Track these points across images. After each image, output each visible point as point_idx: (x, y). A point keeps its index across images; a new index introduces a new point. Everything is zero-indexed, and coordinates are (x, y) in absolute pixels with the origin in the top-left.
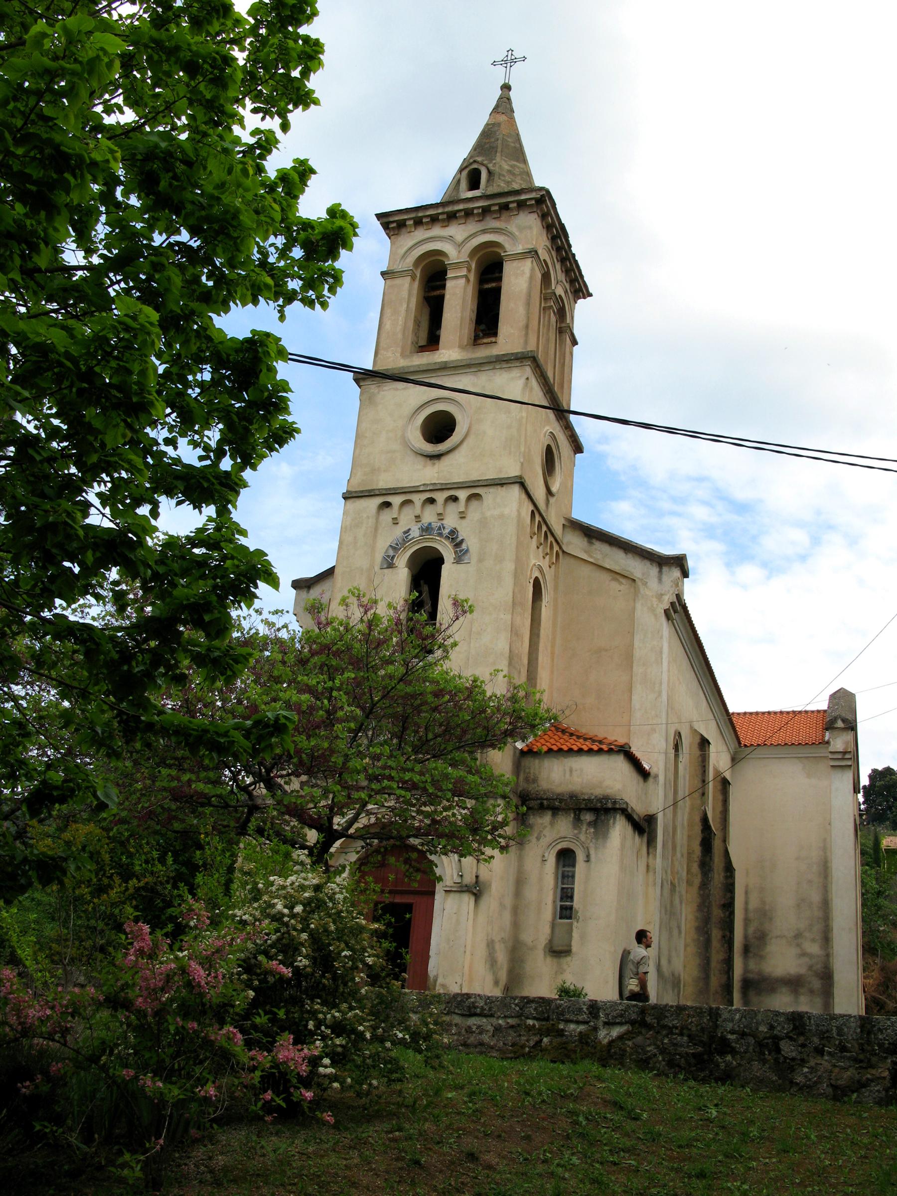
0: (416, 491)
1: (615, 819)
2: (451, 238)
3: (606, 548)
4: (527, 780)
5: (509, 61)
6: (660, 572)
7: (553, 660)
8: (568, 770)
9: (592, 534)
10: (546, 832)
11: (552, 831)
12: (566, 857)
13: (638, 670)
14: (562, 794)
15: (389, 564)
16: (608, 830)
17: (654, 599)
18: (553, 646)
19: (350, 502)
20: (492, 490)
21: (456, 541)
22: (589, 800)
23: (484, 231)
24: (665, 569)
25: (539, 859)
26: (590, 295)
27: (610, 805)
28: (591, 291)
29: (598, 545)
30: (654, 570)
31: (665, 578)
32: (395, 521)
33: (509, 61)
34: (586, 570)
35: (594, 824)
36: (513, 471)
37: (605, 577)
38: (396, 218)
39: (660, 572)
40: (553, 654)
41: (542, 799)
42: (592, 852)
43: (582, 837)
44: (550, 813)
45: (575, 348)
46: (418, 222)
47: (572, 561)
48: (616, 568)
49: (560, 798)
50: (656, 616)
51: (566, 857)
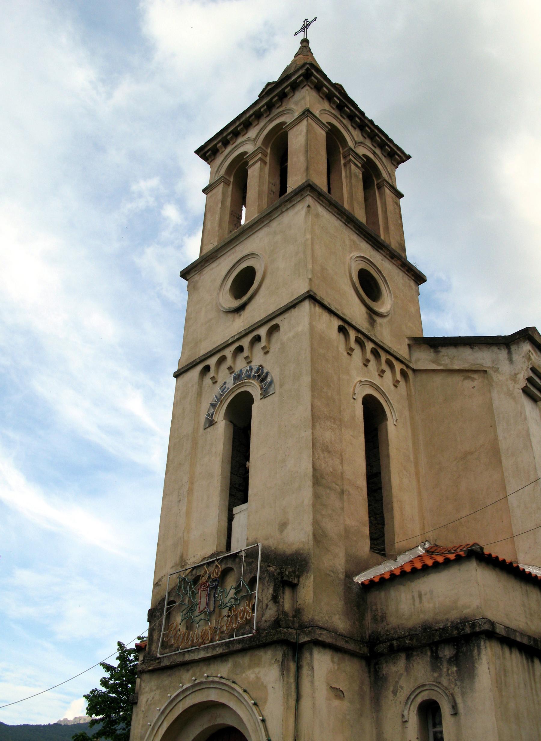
0: (227, 345)
1: (479, 647)
2: (249, 140)
3: (452, 351)
4: (375, 619)
5: (306, 26)
6: (510, 353)
7: (418, 480)
8: (416, 595)
9: (437, 344)
10: (403, 682)
11: (411, 678)
12: (430, 712)
13: (507, 462)
14: (413, 629)
15: (211, 423)
16: (473, 663)
17: (510, 382)
18: (416, 465)
19: (180, 378)
20: (286, 315)
21: (261, 376)
22: (445, 629)
23: (271, 121)
24: (513, 348)
25: (399, 721)
26: (409, 157)
27: (468, 630)
28: (407, 152)
29: (444, 351)
30: (503, 354)
31: (515, 357)
32: (214, 381)
33: (306, 26)
34: (438, 380)
35: (455, 660)
36: (302, 289)
37: (457, 379)
38: (209, 147)
39: (510, 353)
40: (417, 473)
41: (393, 639)
42: (459, 700)
43: (445, 682)
44: (403, 656)
45: (402, 200)
46: (226, 143)
47: (424, 376)
48: (466, 366)
49: (412, 634)
50: (514, 398)
51: (430, 712)
